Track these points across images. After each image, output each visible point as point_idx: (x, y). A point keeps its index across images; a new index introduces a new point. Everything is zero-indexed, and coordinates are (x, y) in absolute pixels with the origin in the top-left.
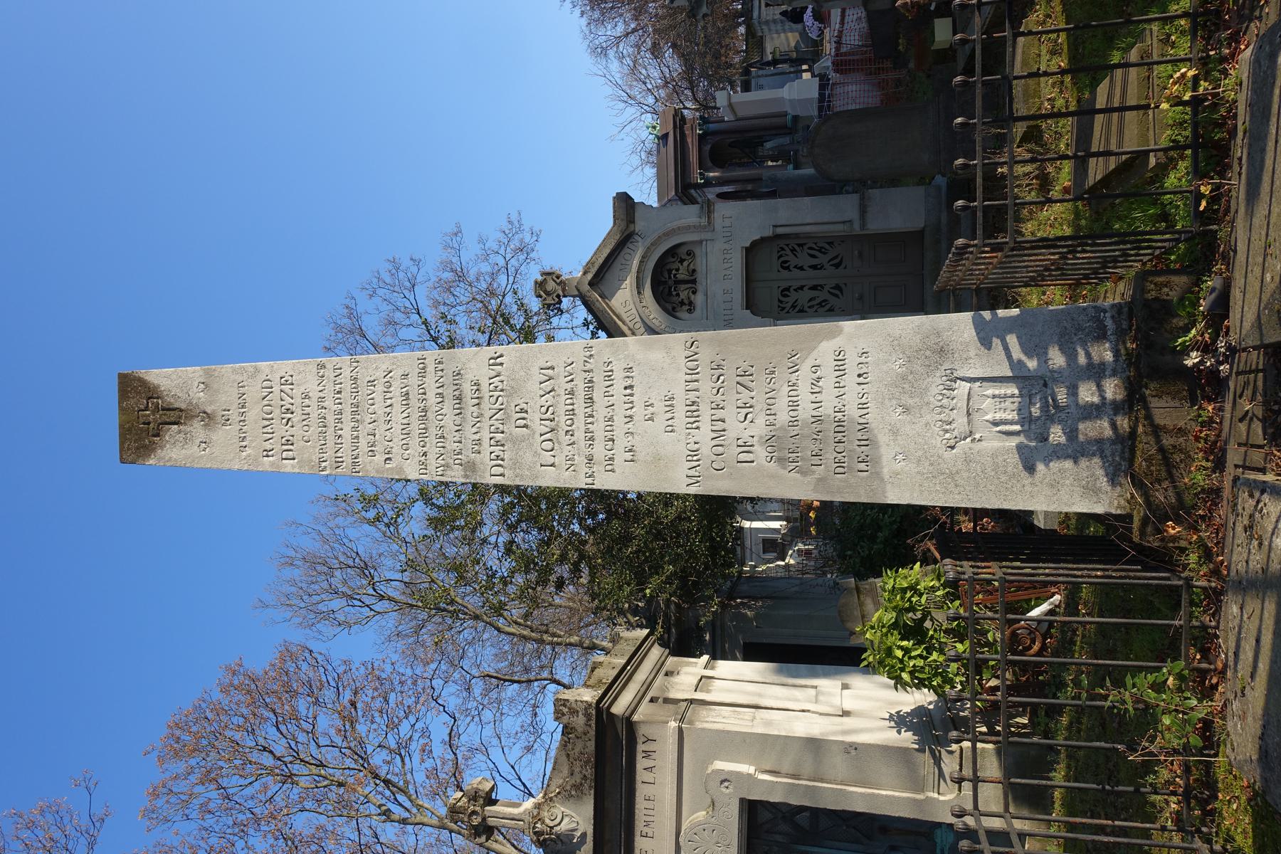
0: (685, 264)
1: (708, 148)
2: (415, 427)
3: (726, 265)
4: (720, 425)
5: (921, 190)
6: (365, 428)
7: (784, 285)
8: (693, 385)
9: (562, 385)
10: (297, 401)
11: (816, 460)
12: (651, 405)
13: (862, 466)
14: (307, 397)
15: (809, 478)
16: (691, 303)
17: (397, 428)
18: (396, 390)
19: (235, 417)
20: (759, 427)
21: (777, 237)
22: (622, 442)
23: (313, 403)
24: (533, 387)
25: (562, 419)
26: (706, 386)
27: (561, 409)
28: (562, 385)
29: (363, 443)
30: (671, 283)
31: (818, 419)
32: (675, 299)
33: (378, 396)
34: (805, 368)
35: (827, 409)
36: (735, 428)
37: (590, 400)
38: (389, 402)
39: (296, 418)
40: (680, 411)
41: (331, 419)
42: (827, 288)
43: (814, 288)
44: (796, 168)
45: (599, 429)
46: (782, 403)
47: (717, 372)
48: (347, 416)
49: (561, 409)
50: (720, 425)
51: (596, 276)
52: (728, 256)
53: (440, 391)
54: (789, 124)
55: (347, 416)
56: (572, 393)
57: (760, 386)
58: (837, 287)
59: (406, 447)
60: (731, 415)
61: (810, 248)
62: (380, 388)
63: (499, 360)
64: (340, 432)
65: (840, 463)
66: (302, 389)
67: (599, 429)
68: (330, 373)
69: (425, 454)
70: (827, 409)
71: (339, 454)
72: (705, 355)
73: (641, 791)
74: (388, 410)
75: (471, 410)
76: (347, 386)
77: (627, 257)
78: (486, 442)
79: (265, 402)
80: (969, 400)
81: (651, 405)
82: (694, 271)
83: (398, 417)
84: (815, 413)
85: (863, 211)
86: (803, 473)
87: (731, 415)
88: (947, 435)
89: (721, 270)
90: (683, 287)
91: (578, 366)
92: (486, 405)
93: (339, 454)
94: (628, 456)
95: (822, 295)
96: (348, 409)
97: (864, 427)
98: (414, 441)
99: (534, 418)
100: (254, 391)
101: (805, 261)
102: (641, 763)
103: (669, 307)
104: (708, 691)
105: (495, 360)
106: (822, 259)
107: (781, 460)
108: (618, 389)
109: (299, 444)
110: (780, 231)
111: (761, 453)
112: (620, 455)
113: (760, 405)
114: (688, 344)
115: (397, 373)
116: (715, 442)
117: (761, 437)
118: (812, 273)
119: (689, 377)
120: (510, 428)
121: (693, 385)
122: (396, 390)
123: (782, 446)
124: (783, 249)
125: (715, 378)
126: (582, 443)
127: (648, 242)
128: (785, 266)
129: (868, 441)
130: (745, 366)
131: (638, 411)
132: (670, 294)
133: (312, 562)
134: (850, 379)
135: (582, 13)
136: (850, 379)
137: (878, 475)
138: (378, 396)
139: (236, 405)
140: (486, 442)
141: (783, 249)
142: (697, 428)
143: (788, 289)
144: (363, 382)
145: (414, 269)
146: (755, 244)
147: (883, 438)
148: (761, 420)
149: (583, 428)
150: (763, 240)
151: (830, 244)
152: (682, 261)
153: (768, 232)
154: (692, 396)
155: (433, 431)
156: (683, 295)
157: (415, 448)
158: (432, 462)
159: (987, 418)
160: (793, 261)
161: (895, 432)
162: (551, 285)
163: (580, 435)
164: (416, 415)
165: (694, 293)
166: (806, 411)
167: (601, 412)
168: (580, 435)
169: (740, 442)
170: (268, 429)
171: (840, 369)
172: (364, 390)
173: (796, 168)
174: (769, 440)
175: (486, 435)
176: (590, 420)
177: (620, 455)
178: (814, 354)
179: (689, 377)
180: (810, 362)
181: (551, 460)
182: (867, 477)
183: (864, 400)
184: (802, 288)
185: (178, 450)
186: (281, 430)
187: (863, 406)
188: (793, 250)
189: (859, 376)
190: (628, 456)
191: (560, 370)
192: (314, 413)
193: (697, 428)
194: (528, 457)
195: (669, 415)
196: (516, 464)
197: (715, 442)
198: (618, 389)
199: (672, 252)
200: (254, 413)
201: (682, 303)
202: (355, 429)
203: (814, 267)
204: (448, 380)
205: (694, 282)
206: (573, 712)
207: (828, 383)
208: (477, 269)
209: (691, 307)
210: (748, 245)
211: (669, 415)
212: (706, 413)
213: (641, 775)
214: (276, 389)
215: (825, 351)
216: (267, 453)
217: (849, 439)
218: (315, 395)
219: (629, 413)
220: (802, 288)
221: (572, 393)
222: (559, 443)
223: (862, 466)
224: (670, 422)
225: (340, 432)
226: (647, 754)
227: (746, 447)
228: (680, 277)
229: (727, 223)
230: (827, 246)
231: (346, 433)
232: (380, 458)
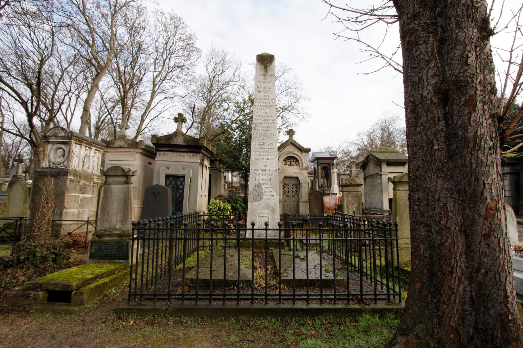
2: (263, 118)
6: (262, 108)
10: (268, 94)
17: (263, 114)
18: (270, 115)
19: (265, 81)
20: (261, 182)
21: (300, 183)
22: (259, 157)
24: (270, 141)
26: (269, 173)
29: (260, 107)
34: (271, 190)
36: (261, 178)
39: (265, 94)
40: (265, 168)
46: (267, 189)
48: (265, 104)
49: (265, 146)
55: (265, 104)
57: (268, 182)
59: (259, 116)
60: (264, 177)
62: (270, 111)
67: (262, 153)
70: (264, 194)
72: (274, 173)
73: (186, 154)
75: (266, 129)
76: (271, 105)
83: (264, 115)
85: (304, 202)
87: (264, 177)
89: (293, 171)
92: (266, 132)
95: (287, 193)
99: (264, 141)
101: (295, 189)
102: (191, 154)
106: (294, 193)
107: (255, 186)
109: (260, 94)
111: (257, 182)
112: (257, 157)
113: (265, 182)
115: (273, 115)
118: (291, 190)
120: (262, 136)
122: (270, 115)
123: (258, 185)
127: (300, 155)
128: (293, 185)
129: (258, 201)
133: (224, 59)
134: (269, 197)
135: (368, 131)
136: (269, 197)
137: (253, 201)
145: (300, 89)
146: (298, 179)
147: (259, 202)
148: (263, 182)
153: (301, 182)
155: (262, 122)
156: (288, 163)
157: (258, 118)
160: (294, 187)
161: (260, 204)
162: (291, 133)
163: (261, 150)
164: (265, 118)
166: (264, 190)
167: (265, 154)
168: (261, 150)
172: (270, 108)
174: (259, 183)
177: (257, 157)
186: (262, 90)
191: (272, 146)
192: (266, 98)
194: (257, 140)
196: (255, 137)
199: (298, 161)
200: (266, 85)
204: (271, 125)
206: (202, 141)
207: (269, 194)
208: (298, 105)
213: (189, 154)
215: (274, 193)
217: (259, 197)
218: (269, 98)
226: (193, 156)
227: (258, 179)
232: (257, 111)
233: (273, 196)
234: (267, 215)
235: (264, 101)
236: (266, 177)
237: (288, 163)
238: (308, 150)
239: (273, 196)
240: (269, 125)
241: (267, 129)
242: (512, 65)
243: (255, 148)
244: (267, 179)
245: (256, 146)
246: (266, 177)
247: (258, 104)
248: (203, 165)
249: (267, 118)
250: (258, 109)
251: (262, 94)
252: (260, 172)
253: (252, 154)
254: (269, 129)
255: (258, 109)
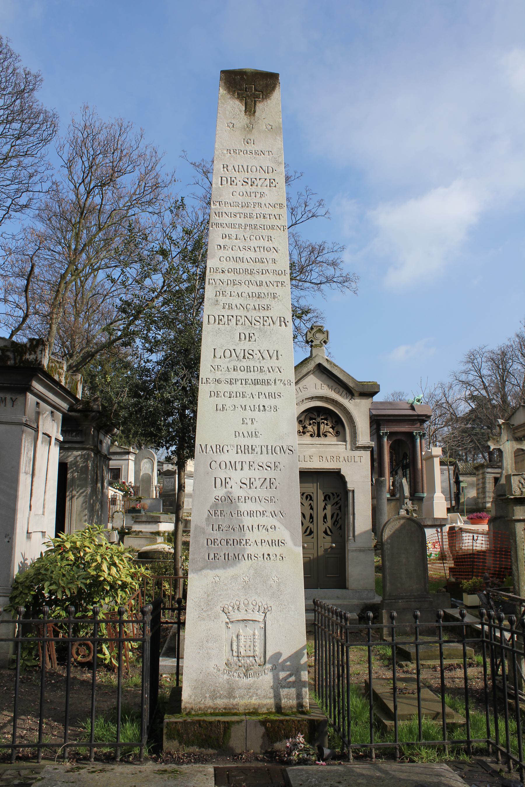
0: (331, 430)
1: (403, 438)
3: (329, 458)
4: (239, 466)
5: (372, 585)
7: (314, 498)
8: (264, 449)
9: (267, 364)
11: (216, 527)
12: (252, 423)
13: (212, 556)
14: (262, 195)
15: (205, 523)
16: (304, 433)
17: (240, 254)
19: (249, 148)
20: (237, 492)
22: (229, 402)
23: (257, 200)
25: (245, 363)
26: (265, 459)
27: (251, 363)
28: (267, 364)
30: (319, 420)
31: (241, 528)
32: (308, 422)
33: (261, 243)
34: (274, 521)
35: (248, 535)
36: (236, 476)
37: (256, 382)
38: (257, 249)
39: (248, 188)
40: (249, 441)
41: (247, 211)
42: (311, 525)
43: (311, 517)
44: (388, 500)
45: (237, 388)
47: (272, 466)
48: (248, 221)
49: (251, 363)
50: (239, 466)
51: (325, 369)
52: (335, 459)
53: (264, 283)
54: (417, 495)
55: (248, 221)
56: (261, 371)
57: (264, 493)
58: (311, 532)
60: (246, 474)
61: (338, 515)
63: (283, 324)
64: (238, 215)
65: (214, 542)
66: (266, 193)
67: (237, 388)
68: (277, 211)
69: (223, 272)
71: (224, 215)
74: (252, 249)
77: (337, 390)
78: (230, 313)
79: (258, 168)
80: (252, 621)
81: (252, 423)
82: (326, 436)
84: (246, 527)
85: (361, 550)
86: (208, 519)
87: (246, 474)
88: (231, 608)
89: (327, 453)
90: (315, 428)
91: (278, 376)
93: (224, 215)
94: (220, 407)
96: (253, 222)
97: (236, 557)
98: (232, 265)
99: (246, 345)
100: (265, 161)
103: (302, 418)
104: (55, 444)
105: (283, 321)
108: (263, 401)
109: (232, 188)
110: (351, 494)
111: (221, 492)
112: (220, 401)
113: (252, 493)
114: (290, 448)
115: (274, 255)
116: (228, 464)
117: (231, 493)
119: (269, 448)
121: (264, 449)
123: (225, 507)
124: (338, 496)
125: (269, 464)
126: (229, 377)
130: (276, 484)
131: (249, 414)
132: (311, 419)
134: (266, 549)
138: (261, 243)
139: (257, 149)
140: (230, 313)
141: (338, 496)
142: (237, 453)
143: (311, 499)
144: (271, 233)
146: (342, 478)
147: (231, 571)
148: (242, 493)
149: (238, 377)
150: (345, 483)
151: (340, 528)
152: (333, 428)
153: (350, 486)
154: (258, 450)
156: (310, 428)
158: (218, 276)
159: (241, 631)
163: (234, 375)
164: (248, 266)
165: (311, 435)
166: (247, 521)
167: (249, 389)
168: (234, 375)
169: (228, 480)
170: (241, 169)
171: (272, 543)
172: (265, 233)
173: (388, 500)
174: (229, 499)
175: (235, 312)
176: (244, 382)
177: (220, 401)
178: (282, 528)
179: (269, 448)
180: (278, 525)
181: (218, 356)
182: (204, 559)
183: (253, 557)
184: (312, 508)
185: (231, 107)
186: (240, 177)
187: (249, 557)
188: (337, 503)
189: (269, 555)
190: (220, 407)
192: (252, 200)
193: (237, 453)
195: (246, 434)
197: (228, 464)
198: (263, 401)
201: (304, 427)
202: (240, 225)
203: (325, 517)
204: (272, 289)
205: (319, 436)
207: (268, 536)
209: (302, 432)
210: (342, 473)
211: (246, 434)
212: (247, 458)
214: (267, 176)
216: (226, 167)
218: (263, 201)
219: (248, 408)
220: (312, 508)
221: (261, 371)
222: (229, 362)
223: (212, 556)
224: (241, 434)
225: (238, 215)
227: (225, 483)
228: (322, 426)
229: (357, 459)
230: (338, 526)
231: (238, 220)
232: (222, 242)
233: (280, 543)
234: (260, 617)
235: (247, 211)
236: (256, 474)
237: (310, 428)
238: (368, 391)
239: (280, 543)
240: (264, 290)
241: (257, 302)
242: (40, 534)
243: (215, 368)
244: (258, 483)
245: (218, 362)
246: (256, 474)
247: (225, 220)
248: (37, 430)
249: (259, 266)
250: (224, 236)
251: (239, 188)
252: (231, 456)
253: (204, 391)
254: (265, 302)
255: (224, 236)
